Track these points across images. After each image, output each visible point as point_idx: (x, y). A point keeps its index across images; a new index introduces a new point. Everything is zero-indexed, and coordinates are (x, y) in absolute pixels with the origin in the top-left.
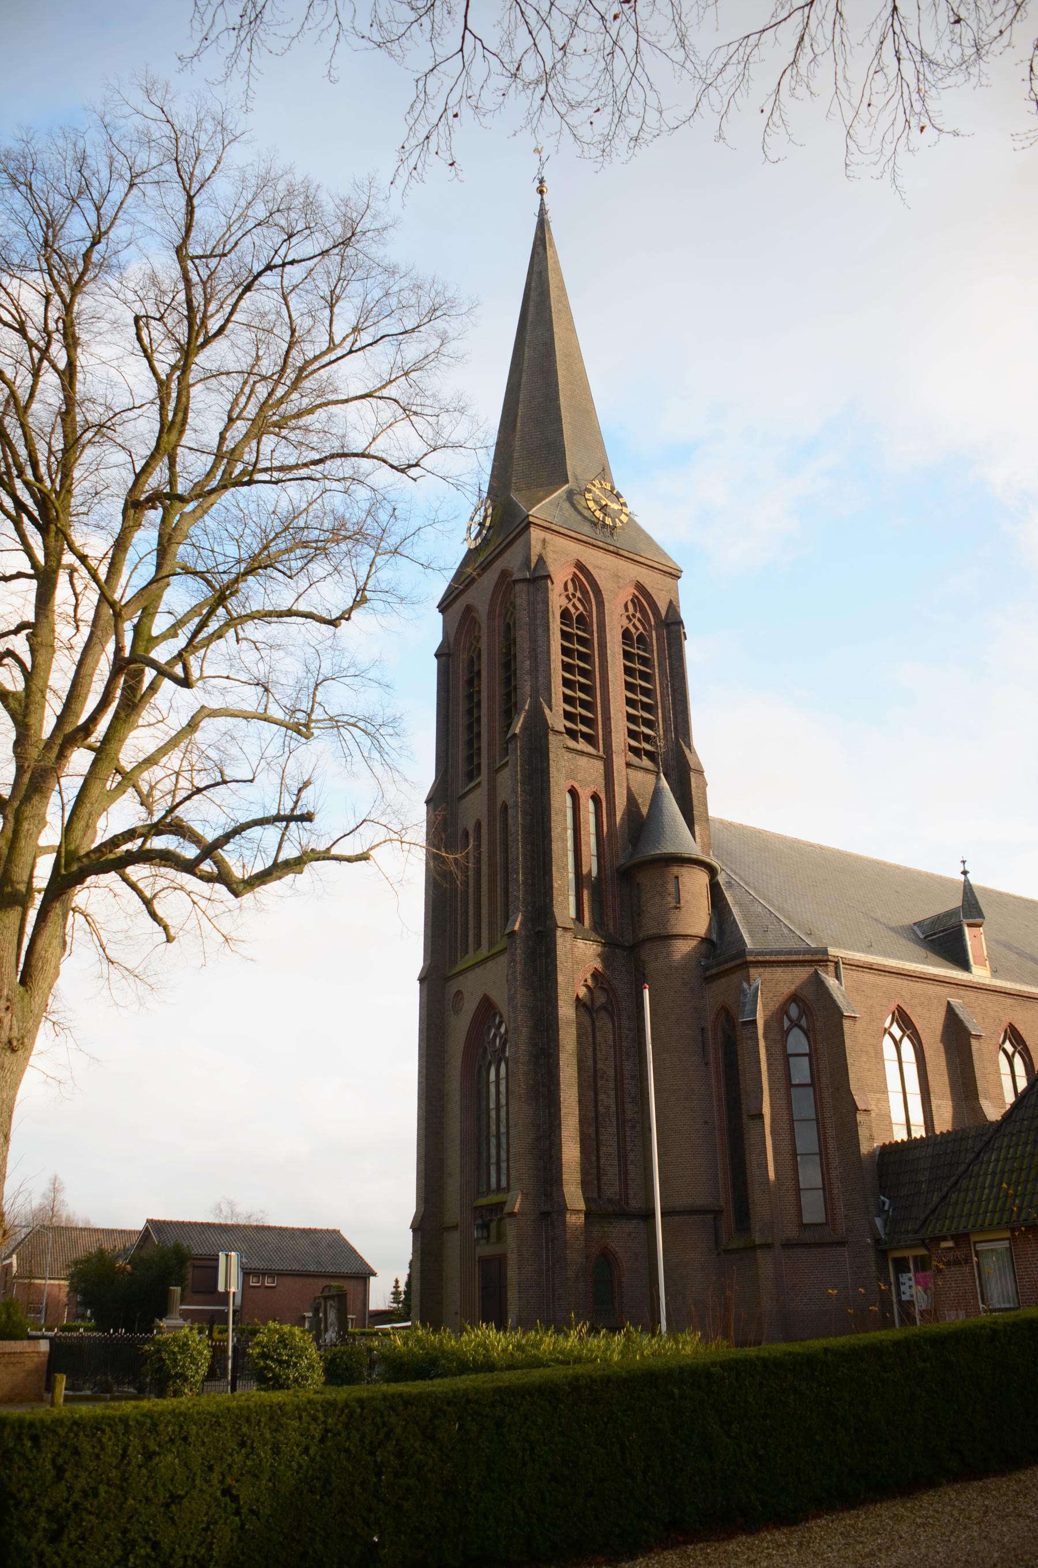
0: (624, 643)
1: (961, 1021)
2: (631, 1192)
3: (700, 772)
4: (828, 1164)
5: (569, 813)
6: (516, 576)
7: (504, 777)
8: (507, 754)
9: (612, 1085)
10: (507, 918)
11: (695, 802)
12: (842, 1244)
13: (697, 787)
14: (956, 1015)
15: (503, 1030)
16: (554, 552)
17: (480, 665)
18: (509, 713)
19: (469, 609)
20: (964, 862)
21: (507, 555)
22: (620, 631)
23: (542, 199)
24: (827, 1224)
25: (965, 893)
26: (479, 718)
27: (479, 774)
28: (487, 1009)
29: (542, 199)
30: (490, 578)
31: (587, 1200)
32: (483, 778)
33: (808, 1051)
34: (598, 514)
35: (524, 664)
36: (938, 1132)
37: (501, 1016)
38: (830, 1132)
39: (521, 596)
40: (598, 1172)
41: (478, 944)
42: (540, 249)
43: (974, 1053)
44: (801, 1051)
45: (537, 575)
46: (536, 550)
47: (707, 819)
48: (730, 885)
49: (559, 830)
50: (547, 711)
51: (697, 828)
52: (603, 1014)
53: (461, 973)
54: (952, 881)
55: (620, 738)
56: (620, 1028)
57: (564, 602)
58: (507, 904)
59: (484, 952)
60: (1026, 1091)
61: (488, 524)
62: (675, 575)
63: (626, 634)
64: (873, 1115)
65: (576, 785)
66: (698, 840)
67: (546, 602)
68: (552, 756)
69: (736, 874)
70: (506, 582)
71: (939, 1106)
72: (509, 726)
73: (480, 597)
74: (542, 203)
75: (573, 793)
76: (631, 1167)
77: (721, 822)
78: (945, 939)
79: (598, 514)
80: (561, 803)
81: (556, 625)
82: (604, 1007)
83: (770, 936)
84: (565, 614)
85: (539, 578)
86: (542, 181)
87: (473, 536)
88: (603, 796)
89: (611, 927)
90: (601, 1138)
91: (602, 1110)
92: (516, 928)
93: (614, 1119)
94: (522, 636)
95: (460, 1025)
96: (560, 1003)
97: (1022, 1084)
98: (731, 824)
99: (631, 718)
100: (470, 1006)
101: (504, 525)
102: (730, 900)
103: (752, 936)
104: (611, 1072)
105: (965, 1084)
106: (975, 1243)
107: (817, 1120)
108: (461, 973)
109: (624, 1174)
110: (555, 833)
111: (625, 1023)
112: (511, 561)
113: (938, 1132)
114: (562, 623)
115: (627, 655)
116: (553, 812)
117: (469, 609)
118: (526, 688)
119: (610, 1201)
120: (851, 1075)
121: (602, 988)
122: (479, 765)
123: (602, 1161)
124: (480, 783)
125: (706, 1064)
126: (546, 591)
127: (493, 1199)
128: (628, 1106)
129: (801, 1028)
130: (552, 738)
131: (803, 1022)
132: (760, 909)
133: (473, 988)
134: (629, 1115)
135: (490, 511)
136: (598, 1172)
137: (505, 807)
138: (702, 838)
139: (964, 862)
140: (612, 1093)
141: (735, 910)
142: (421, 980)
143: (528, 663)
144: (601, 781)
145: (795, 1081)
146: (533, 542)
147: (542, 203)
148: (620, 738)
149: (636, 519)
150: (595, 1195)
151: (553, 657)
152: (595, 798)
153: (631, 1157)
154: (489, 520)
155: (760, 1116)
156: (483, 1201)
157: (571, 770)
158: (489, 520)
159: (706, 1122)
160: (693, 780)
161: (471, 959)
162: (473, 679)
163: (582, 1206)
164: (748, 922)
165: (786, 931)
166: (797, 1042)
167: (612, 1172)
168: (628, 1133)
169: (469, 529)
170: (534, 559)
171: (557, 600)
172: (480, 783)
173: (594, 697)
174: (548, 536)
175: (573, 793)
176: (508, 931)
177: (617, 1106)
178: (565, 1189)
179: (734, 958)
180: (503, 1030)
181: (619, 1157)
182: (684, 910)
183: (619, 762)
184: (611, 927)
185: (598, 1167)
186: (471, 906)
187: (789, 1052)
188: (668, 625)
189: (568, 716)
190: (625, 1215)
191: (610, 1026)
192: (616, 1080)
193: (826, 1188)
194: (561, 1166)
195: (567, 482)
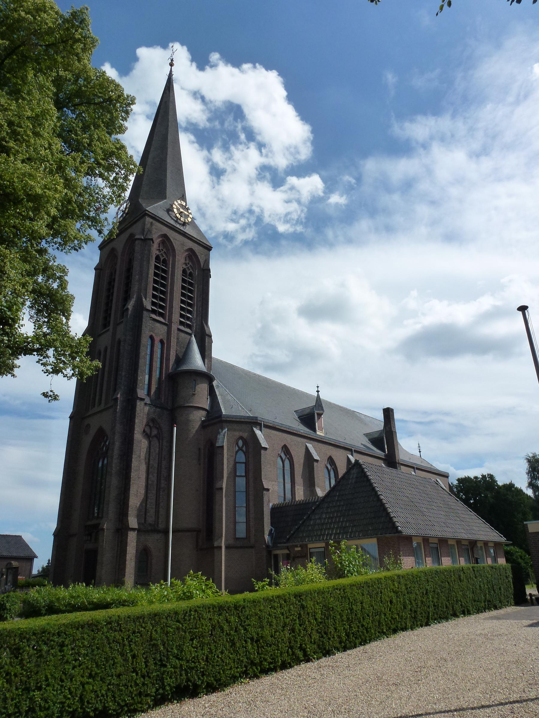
0: (183, 275)
1: (311, 453)
2: (160, 520)
3: (210, 336)
4: (249, 512)
5: (149, 347)
6: (137, 237)
7: (121, 328)
8: (123, 318)
9: (156, 471)
10: (115, 391)
11: (207, 349)
12: (252, 547)
13: (208, 342)
14: (309, 451)
15: (107, 443)
16: (156, 229)
17: (115, 276)
18: (126, 299)
19: (113, 250)
20: (318, 387)
21: (134, 226)
22: (182, 269)
23: (171, 69)
24: (246, 538)
25: (317, 400)
26: (112, 300)
27: (109, 326)
28: (101, 434)
29: (171, 69)
30: (125, 236)
31: (139, 524)
32: (111, 327)
33: (244, 461)
34: (178, 215)
35: (136, 277)
36: (297, 500)
37: (107, 437)
38: (251, 497)
39: (138, 247)
40: (146, 511)
41: (100, 403)
42: (167, 92)
43: (315, 467)
44: (241, 461)
45: (146, 237)
46: (148, 226)
47: (211, 357)
48: (218, 386)
49: (143, 354)
50: (144, 300)
51: (206, 360)
52: (155, 439)
53: (90, 416)
54: (311, 396)
55: (176, 317)
56: (162, 446)
57: (158, 253)
58: (116, 384)
59: (102, 406)
60: (335, 486)
61: (126, 212)
62: (209, 248)
63: (184, 271)
64: (270, 491)
65: (154, 335)
66: (206, 365)
67: (149, 251)
68: (144, 320)
69: (221, 382)
70: (132, 239)
71: (298, 489)
72: (124, 305)
73: (119, 245)
74: (171, 71)
75: (152, 338)
76: (161, 509)
77: (217, 360)
78: (309, 418)
79: (178, 215)
80: (145, 341)
81: (153, 262)
82: (155, 436)
83: (233, 410)
84: (157, 258)
85: (148, 241)
86: (172, 60)
87: (119, 216)
88: (165, 341)
89: (163, 400)
90: (149, 495)
91: (150, 482)
92: (119, 396)
93: (155, 487)
94: (136, 265)
95: (87, 440)
96: (135, 432)
97: (333, 483)
98: (221, 361)
99: (182, 309)
100: (93, 431)
101: (135, 214)
102: (217, 393)
103: (225, 409)
104: (156, 465)
105: (310, 482)
106: (310, 549)
107: (246, 492)
108: (90, 416)
109: (157, 512)
110: (142, 354)
111: (165, 443)
112: (136, 230)
113: (297, 500)
114: (156, 262)
115: (184, 281)
116: (141, 345)
117: (113, 250)
118: (135, 288)
119: (150, 524)
120: (262, 473)
121: (156, 427)
122: (109, 322)
123: (148, 506)
124: (109, 329)
125: (200, 464)
126: (150, 246)
127: (94, 522)
128: (162, 481)
129: (243, 451)
130: (145, 312)
131: (244, 449)
132: (230, 398)
133: (95, 423)
134: (163, 485)
135: (128, 206)
136: (146, 511)
137: (119, 342)
138: (208, 365)
139: (318, 387)
140: (155, 475)
141: (219, 397)
142: (71, 418)
143: (137, 277)
144: (165, 334)
145: (238, 474)
146: (146, 223)
147: (171, 71)
148: (176, 317)
149: (195, 221)
150: (143, 521)
151: (150, 276)
152: (162, 341)
153: (161, 504)
154: (127, 210)
155: (221, 489)
156: (89, 523)
157: (152, 328)
158: (127, 210)
159: (197, 491)
160: (207, 339)
161: (96, 409)
162: (111, 284)
163: (136, 526)
164: (224, 403)
165: (240, 408)
166: (241, 457)
167: (152, 512)
168: (161, 494)
169: (117, 213)
170: (146, 230)
171: (155, 249)
172: (109, 329)
173: (167, 297)
174: (154, 222)
175: (152, 338)
176: (114, 397)
177: (157, 481)
178: (129, 518)
179: (217, 417)
180: (107, 443)
181: (156, 505)
182: (196, 395)
183: (175, 326)
184: (163, 400)
185: (146, 509)
186: (99, 385)
187: (237, 461)
188: (203, 270)
189: (153, 304)
190: (158, 531)
191: (158, 444)
192: (158, 470)
193: (248, 522)
194: (128, 507)
195: (165, 198)
